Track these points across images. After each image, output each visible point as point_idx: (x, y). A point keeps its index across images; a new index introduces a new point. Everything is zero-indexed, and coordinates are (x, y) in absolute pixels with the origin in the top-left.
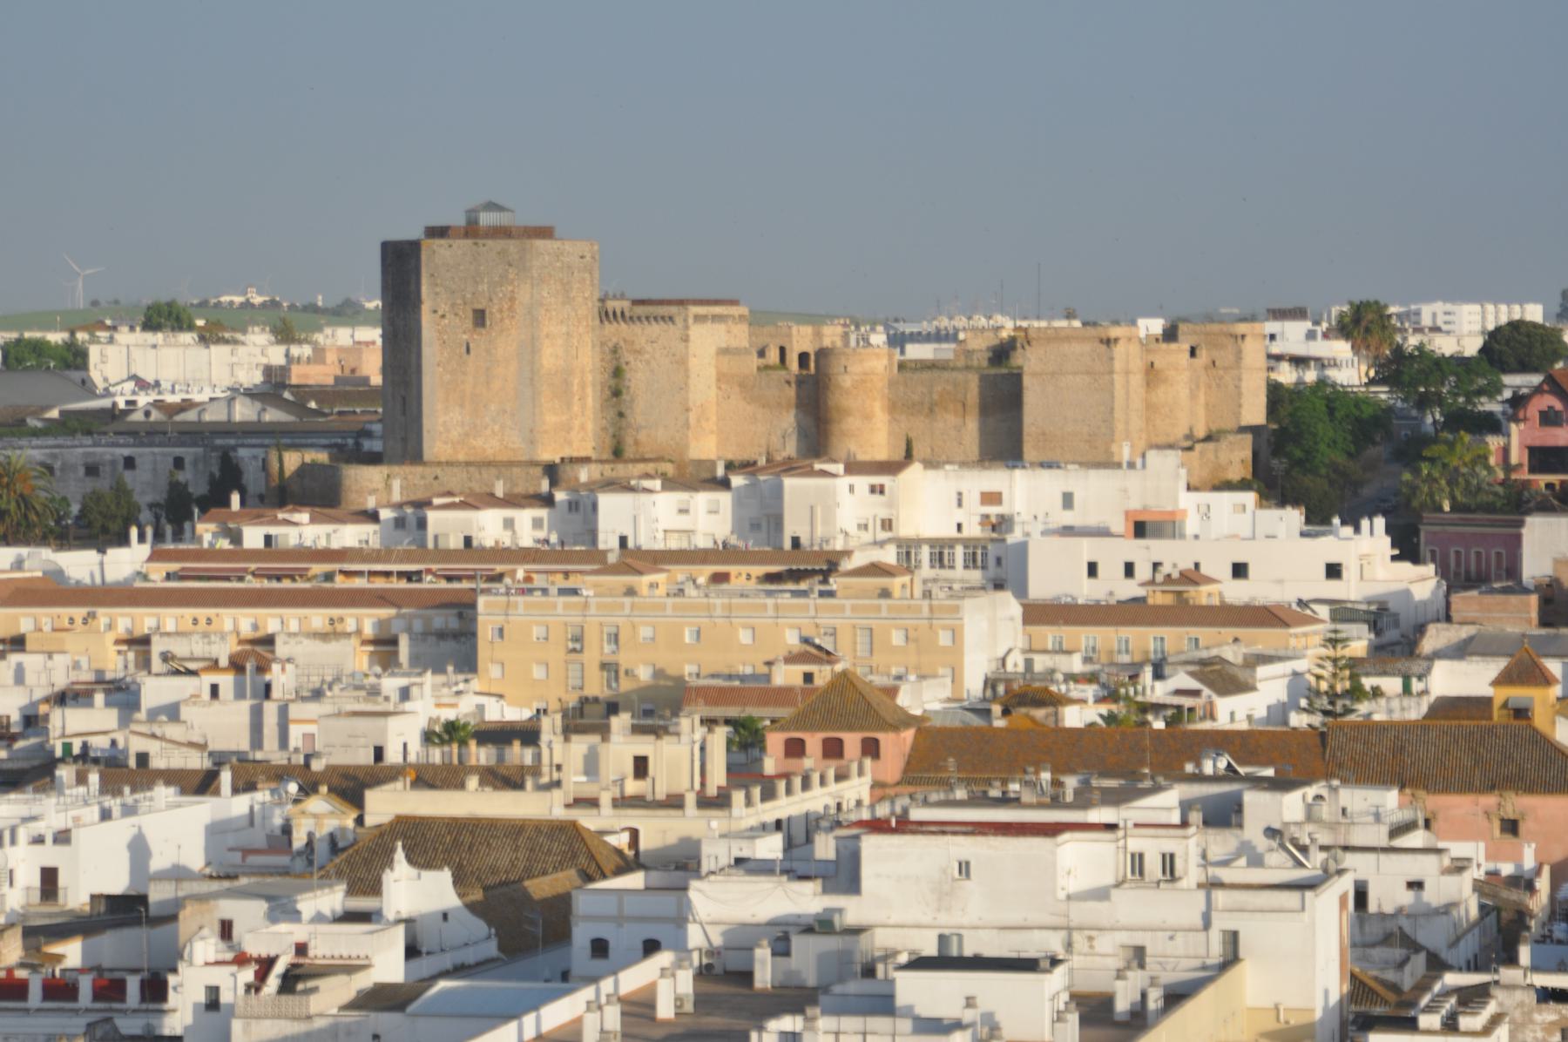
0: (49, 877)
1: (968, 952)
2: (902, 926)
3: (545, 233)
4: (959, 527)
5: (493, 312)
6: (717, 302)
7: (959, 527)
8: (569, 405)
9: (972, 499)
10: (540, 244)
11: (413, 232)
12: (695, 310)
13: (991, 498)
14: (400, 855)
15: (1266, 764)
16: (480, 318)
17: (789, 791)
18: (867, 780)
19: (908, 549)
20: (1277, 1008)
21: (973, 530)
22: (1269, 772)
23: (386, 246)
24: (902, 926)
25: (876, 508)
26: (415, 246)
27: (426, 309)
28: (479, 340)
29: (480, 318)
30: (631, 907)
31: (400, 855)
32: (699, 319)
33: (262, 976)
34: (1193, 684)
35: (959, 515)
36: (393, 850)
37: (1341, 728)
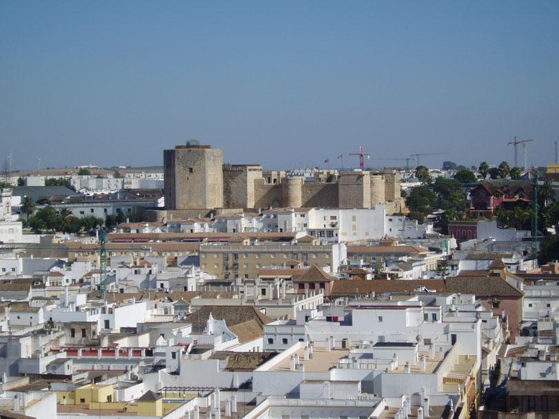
0: (107, 323)
1: (386, 341)
2: (465, 322)
3: (208, 147)
4: (325, 226)
5: (195, 168)
6: (254, 165)
7: (325, 226)
8: (215, 194)
9: (328, 219)
10: (207, 150)
11: (172, 148)
12: (249, 168)
13: (334, 218)
14: (211, 315)
15: (434, 289)
16: (191, 170)
17: (94, 314)
18: (323, 295)
19: (312, 232)
20: (467, 356)
21: (328, 227)
22: (435, 291)
23: (164, 151)
24: (465, 322)
25: (303, 220)
26: (173, 151)
27: (176, 168)
28: (191, 176)
29: (191, 170)
30: (279, 330)
31: (211, 315)
32: (250, 170)
33: (186, 349)
34: (397, 268)
35: (325, 223)
36: (209, 314)
37: (450, 278)
